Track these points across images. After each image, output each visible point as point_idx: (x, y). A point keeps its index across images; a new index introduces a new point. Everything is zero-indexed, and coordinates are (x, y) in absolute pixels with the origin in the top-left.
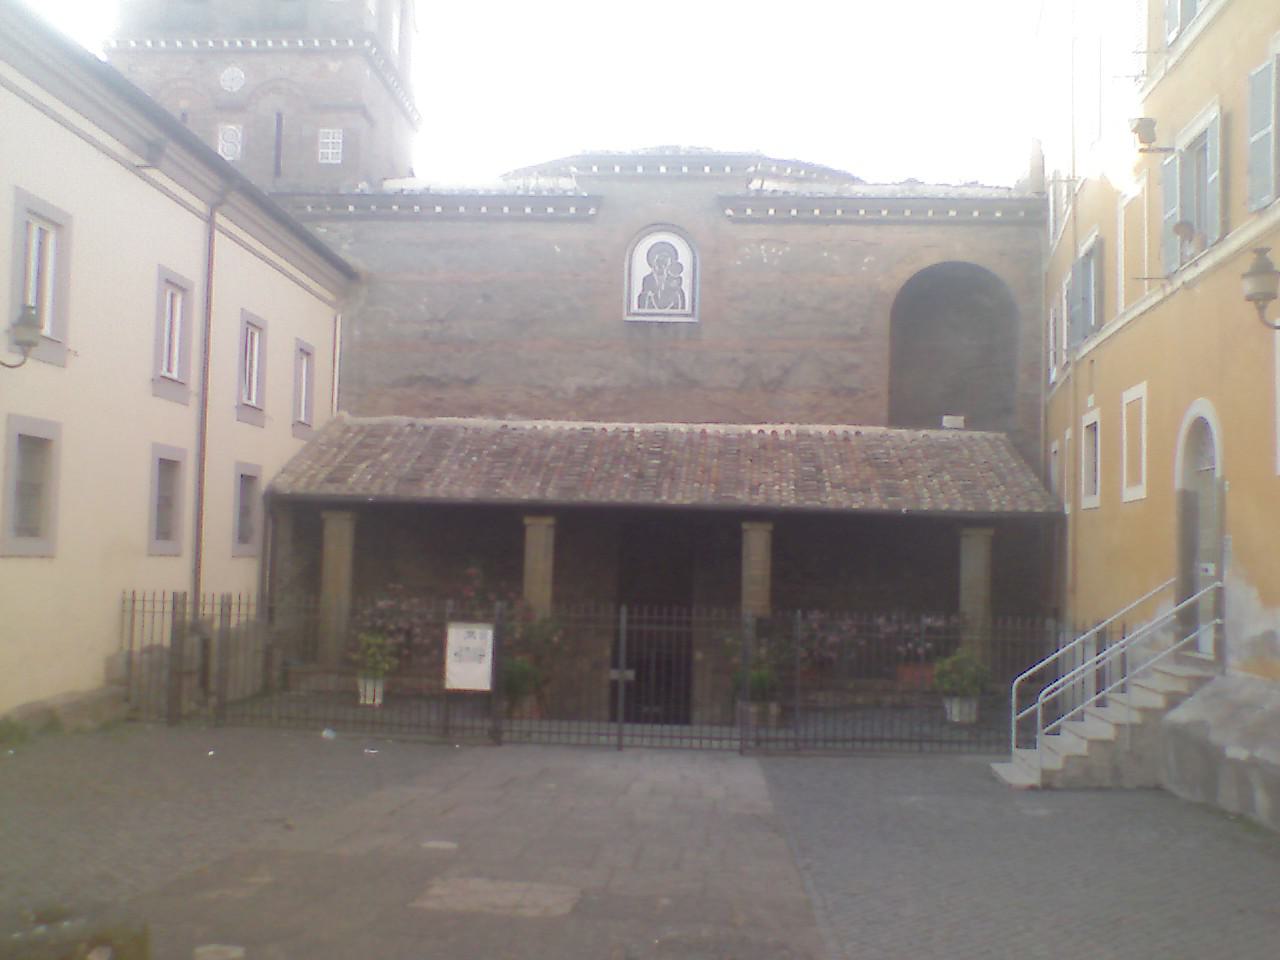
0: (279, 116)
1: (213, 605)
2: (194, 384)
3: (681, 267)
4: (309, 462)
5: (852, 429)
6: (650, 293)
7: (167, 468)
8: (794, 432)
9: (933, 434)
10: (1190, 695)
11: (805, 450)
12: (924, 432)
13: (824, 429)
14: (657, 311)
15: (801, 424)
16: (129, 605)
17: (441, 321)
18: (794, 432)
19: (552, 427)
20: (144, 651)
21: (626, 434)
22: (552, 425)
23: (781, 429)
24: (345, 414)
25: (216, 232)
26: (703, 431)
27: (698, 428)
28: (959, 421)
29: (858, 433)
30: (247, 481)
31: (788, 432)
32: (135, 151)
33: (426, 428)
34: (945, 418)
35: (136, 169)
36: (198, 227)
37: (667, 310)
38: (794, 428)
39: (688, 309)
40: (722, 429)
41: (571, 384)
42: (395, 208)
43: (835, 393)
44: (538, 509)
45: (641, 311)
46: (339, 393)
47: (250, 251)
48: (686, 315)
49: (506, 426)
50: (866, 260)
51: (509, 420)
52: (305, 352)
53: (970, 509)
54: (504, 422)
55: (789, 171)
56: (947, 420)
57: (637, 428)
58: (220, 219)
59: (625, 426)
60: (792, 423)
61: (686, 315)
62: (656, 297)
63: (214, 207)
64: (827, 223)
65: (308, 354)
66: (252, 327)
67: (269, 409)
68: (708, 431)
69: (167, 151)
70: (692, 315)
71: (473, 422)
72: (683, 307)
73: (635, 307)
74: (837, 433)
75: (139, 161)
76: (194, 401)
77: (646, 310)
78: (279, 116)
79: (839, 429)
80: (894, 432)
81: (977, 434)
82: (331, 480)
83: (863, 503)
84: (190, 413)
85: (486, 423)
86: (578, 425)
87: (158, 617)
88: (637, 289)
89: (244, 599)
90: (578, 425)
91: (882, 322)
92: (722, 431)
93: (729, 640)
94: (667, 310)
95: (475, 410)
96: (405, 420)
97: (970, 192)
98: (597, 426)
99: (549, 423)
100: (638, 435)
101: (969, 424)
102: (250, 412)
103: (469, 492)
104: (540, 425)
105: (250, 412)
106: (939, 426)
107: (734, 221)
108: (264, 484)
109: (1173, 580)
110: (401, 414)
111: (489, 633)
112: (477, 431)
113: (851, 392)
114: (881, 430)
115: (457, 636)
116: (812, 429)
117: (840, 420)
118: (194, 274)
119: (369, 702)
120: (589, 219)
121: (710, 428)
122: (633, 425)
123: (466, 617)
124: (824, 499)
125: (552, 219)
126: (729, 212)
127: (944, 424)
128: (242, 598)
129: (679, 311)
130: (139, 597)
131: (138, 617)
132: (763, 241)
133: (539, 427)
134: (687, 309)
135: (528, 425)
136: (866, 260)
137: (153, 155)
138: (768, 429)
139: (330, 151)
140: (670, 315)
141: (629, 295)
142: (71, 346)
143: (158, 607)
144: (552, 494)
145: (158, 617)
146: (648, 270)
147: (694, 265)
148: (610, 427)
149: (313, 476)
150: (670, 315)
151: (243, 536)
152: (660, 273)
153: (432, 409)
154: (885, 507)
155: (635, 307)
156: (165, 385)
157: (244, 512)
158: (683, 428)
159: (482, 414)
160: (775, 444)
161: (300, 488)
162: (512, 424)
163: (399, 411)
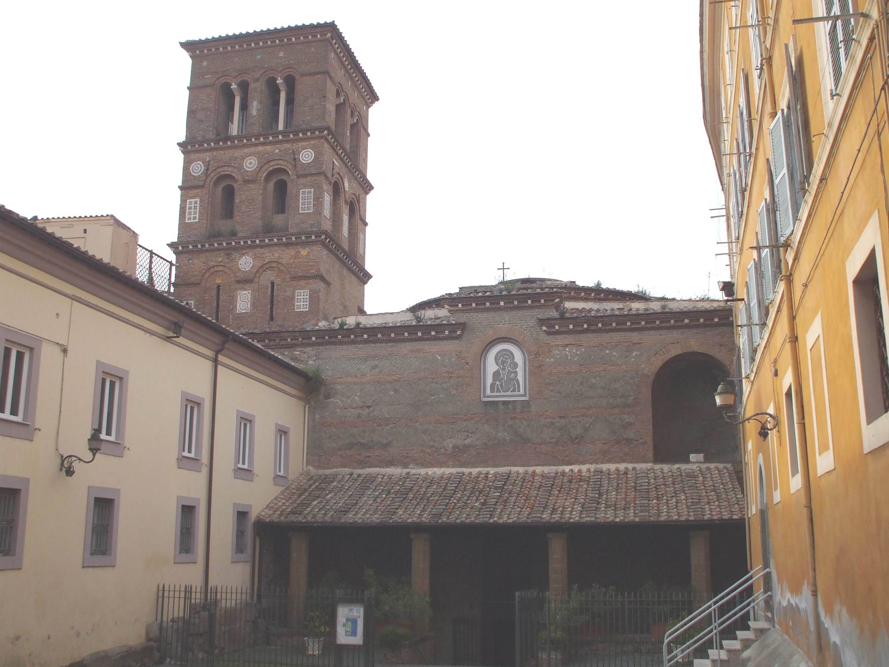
0: (273, 284)
1: (164, 591)
2: (205, 459)
3: (516, 365)
4: (284, 501)
5: (630, 466)
6: (497, 383)
7: (188, 511)
8: (592, 470)
9: (684, 467)
10: (757, 640)
11: (597, 481)
12: (677, 466)
13: (612, 467)
14: (502, 393)
15: (597, 464)
16: (161, 594)
17: (369, 407)
18: (592, 470)
19: (438, 472)
20: (173, 620)
21: (483, 476)
22: (438, 471)
23: (584, 468)
24: (310, 468)
25: (219, 367)
26: (534, 472)
27: (531, 469)
28: (701, 457)
29: (634, 469)
30: (242, 515)
31: (589, 470)
32: (169, 329)
33: (359, 476)
34: (691, 456)
35: (168, 339)
36: (208, 365)
37: (509, 393)
38: (592, 467)
39: (522, 391)
40: (546, 469)
41: (449, 443)
42: (340, 337)
43: (618, 442)
44: (418, 528)
45: (492, 394)
46: (307, 454)
47: (703, 58)
48: (521, 396)
49: (409, 473)
50: (634, 354)
51: (411, 468)
52: (282, 432)
53: (692, 518)
54: (408, 470)
55: (593, 295)
56: (693, 457)
57: (492, 471)
58: (221, 358)
59: (484, 470)
60: (592, 464)
61: (521, 396)
62: (501, 385)
63: (217, 352)
64: (607, 331)
65: (285, 433)
66: (245, 421)
67: (256, 470)
68: (537, 471)
69: (185, 325)
70: (525, 395)
71: (390, 470)
72: (519, 391)
73: (488, 392)
74: (620, 469)
75: (171, 334)
76: (205, 470)
77: (495, 394)
78: (273, 284)
79: (622, 466)
80: (658, 467)
81: (712, 466)
82: (293, 512)
83: (622, 518)
84: (203, 476)
85: (396, 471)
86: (453, 470)
87: (177, 600)
88: (489, 380)
89: (244, 591)
90: (453, 470)
91: (646, 394)
92: (546, 471)
93: (386, 608)
94: (509, 393)
95: (391, 463)
96: (347, 470)
97: (700, 305)
98: (466, 470)
99: (436, 470)
100: (491, 476)
101: (707, 460)
102: (244, 473)
103: (376, 519)
104: (430, 471)
105: (244, 473)
106: (687, 461)
107: (548, 333)
108: (253, 517)
109: (761, 566)
110: (345, 467)
111: (362, 610)
112: (390, 477)
113: (628, 441)
114: (650, 465)
115: (343, 613)
116: (605, 467)
117: (624, 461)
118: (203, 391)
119: (310, 652)
120: (458, 338)
121: (539, 469)
122: (488, 469)
123: (350, 601)
124: (598, 516)
125: (435, 339)
126: (544, 328)
127: (691, 459)
128: (238, 588)
129: (517, 393)
130: (166, 588)
131: (166, 600)
132: (567, 345)
133: (430, 473)
134: (521, 392)
135: (422, 471)
136: (634, 354)
137: (177, 329)
138: (576, 468)
139: (302, 303)
140: (510, 396)
141: (485, 384)
142: (127, 444)
143: (177, 594)
144: (426, 518)
145: (177, 600)
146: (496, 368)
147: (525, 363)
148: (475, 471)
149: (284, 510)
150: (510, 396)
151: (239, 548)
152: (504, 369)
153: (363, 464)
154: (637, 519)
155: (488, 392)
156: (186, 462)
157: (240, 534)
158: (521, 470)
159: (394, 465)
160: (581, 478)
161: (275, 518)
162: (413, 471)
163: (344, 466)
